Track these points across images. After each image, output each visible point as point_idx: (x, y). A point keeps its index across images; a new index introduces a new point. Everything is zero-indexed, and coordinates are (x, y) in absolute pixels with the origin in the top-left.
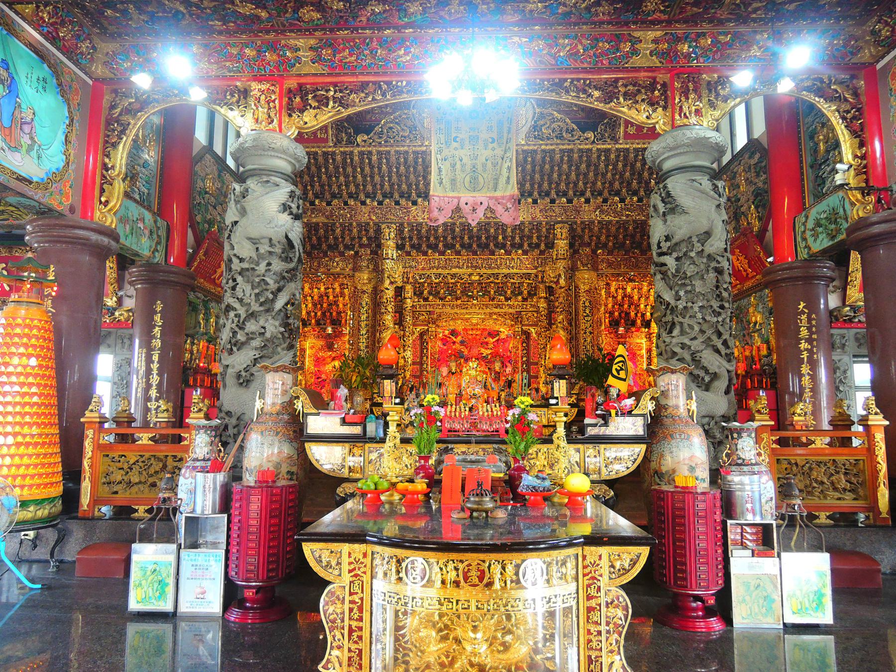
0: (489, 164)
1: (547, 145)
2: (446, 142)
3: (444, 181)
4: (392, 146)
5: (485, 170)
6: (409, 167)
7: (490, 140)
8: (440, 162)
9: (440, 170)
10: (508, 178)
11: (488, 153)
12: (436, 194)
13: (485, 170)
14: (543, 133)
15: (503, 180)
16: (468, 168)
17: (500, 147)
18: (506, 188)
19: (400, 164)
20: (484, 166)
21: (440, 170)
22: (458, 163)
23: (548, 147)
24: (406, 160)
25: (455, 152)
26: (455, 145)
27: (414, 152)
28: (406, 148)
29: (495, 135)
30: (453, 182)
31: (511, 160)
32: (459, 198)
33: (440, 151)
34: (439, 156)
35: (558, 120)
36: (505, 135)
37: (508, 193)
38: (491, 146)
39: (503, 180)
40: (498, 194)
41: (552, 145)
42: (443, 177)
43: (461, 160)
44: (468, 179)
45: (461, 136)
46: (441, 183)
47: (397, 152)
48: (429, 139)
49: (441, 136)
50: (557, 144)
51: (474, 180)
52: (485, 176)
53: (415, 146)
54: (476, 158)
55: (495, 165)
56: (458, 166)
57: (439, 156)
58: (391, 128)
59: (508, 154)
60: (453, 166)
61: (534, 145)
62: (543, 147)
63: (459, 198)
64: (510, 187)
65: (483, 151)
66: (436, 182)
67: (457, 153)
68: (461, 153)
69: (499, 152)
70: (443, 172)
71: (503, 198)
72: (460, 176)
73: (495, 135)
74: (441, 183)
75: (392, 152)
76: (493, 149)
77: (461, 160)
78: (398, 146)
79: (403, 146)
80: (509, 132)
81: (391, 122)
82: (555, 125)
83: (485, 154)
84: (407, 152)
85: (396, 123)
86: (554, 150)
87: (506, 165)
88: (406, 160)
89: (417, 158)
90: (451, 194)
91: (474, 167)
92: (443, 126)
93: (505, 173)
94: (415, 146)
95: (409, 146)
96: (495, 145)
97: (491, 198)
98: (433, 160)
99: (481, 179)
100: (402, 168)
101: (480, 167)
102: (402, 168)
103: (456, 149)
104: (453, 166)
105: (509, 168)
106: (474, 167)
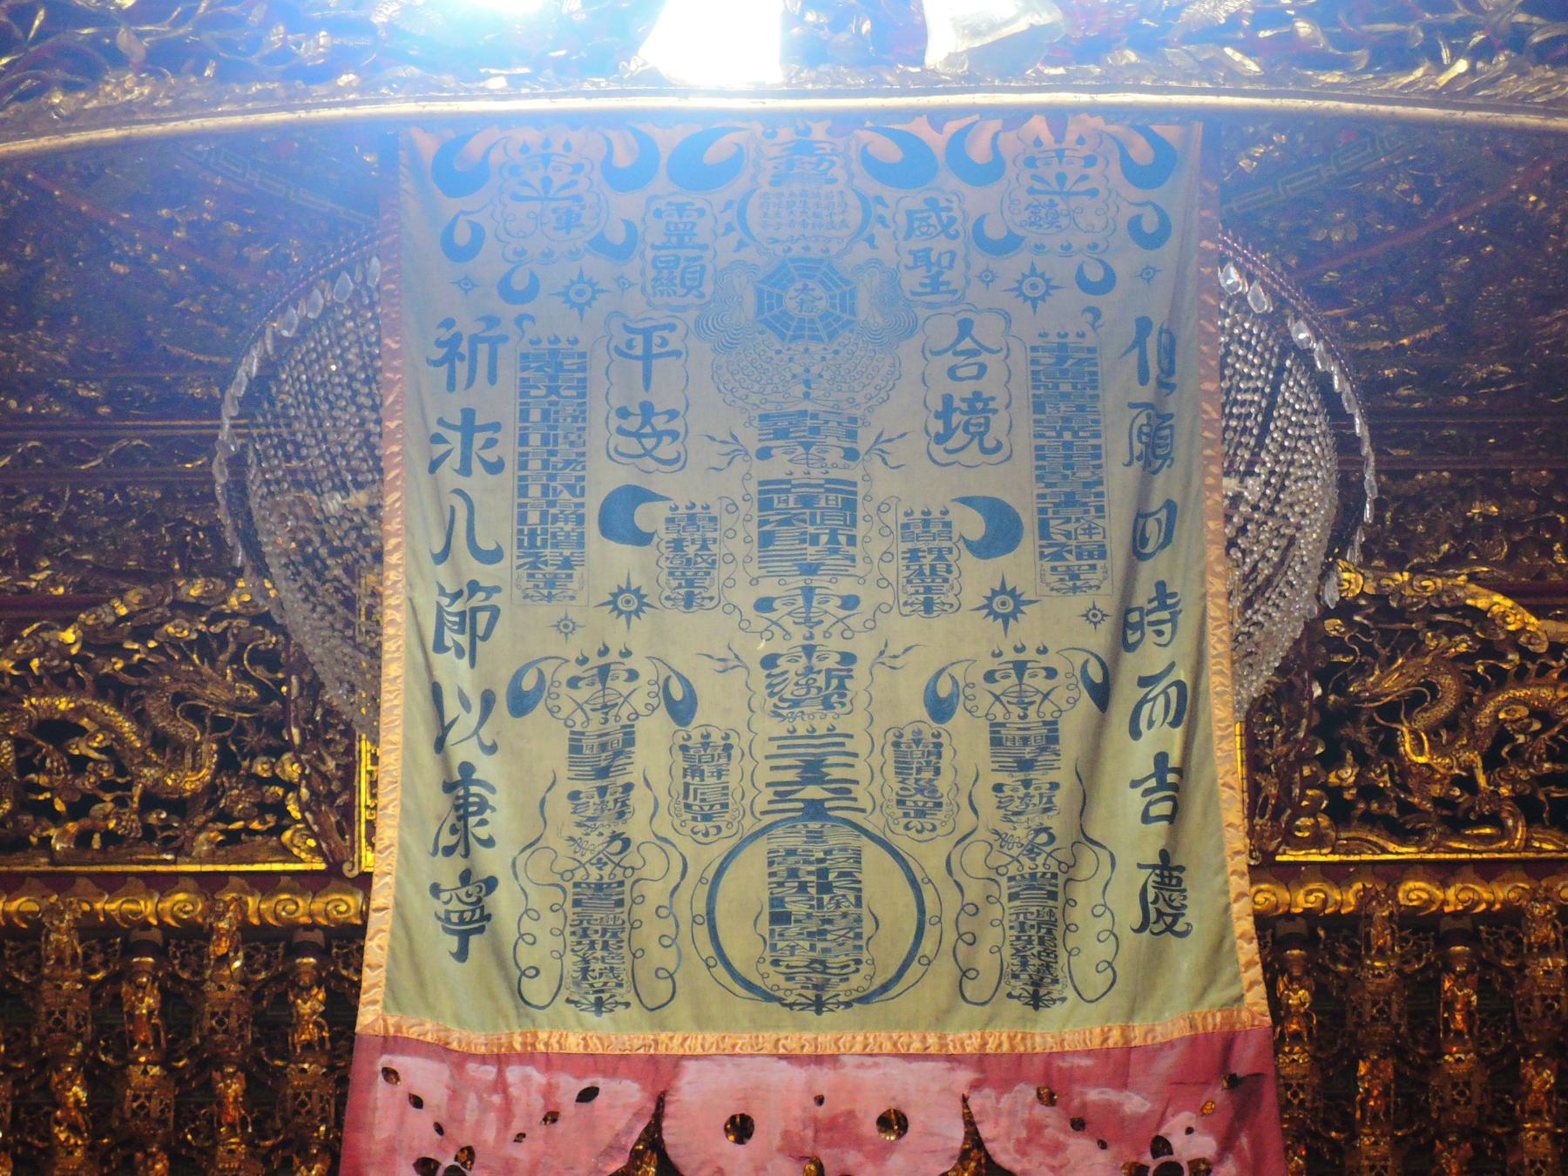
0: (966, 741)
1: (1444, 873)
2: (530, 543)
3: (504, 903)
4: (60, 882)
5: (922, 805)
6: (207, 1063)
7: (973, 525)
8: (464, 722)
9: (461, 792)
10: (1168, 871)
11: (960, 640)
12: (425, 1028)
13: (922, 805)
14: (1403, 772)
15: (1108, 900)
16: (752, 781)
17: (1073, 582)
18: (1153, 965)
19: (123, 1047)
20: (917, 759)
21: (461, 792)
22: (655, 731)
23: (1453, 897)
24: (180, 1002)
25: (617, 633)
26: (616, 562)
27: (253, 936)
28: (181, 903)
29: (1016, 485)
30: (600, 910)
31: (1186, 709)
32: (659, 1075)
33: (471, 623)
34: (455, 673)
35: (1534, 666)
36: (1119, 479)
37: (1170, 1019)
38: (976, 577)
39: (1108, 900)
40: (1069, 1028)
41: (1488, 871)
42: (490, 862)
43: (682, 710)
44: (749, 882)
45: (677, 488)
46: (471, 923)
47: (96, 932)
48: (368, 468)
49: (476, 484)
50: (1538, 869)
51: (815, 896)
52: (930, 857)
53: (266, 884)
54: (835, 692)
55: (1022, 752)
56: (654, 756)
57: (455, 673)
58: (61, 730)
59: (1151, 656)
60: (603, 760)
61: (1337, 875)
62: (1414, 891)
63: (659, 1075)
64: (1186, 957)
65: (905, 628)
66: (424, 910)
67: (637, 636)
68: (686, 641)
69: (1066, 629)
70: (502, 821)
71: (1120, 1065)
72: (665, 855)
73: (1016, 485)
74: (471, 923)
75: (61, 937)
76: (1005, 605)
77: (682, 710)
78: (111, 884)
79: (162, 884)
80: (1154, 450)
81: (60, 681)
82: (1502, 707)
83: (909, 651)
84: (192, 936)
85: (108, 688)
86: (1510, 918)
87: (1138, 758)
88: (180, 1002)
89: (288, 983)
90: (577, 1032)
91: (813, 771)
92: (497, 401)
93: (1128, 829)
94: (266, 884)
95: (209, 884)
96: (1021, 566)
97: (996, 1071)
98: (392, 698)
99: (881, 883)
100: (146, 1072)
101: (873, 783)
102: (146, 1072)
103: (627, 602)
104: (603, 760)
105: (1173, 784)
106: (813, 771)
